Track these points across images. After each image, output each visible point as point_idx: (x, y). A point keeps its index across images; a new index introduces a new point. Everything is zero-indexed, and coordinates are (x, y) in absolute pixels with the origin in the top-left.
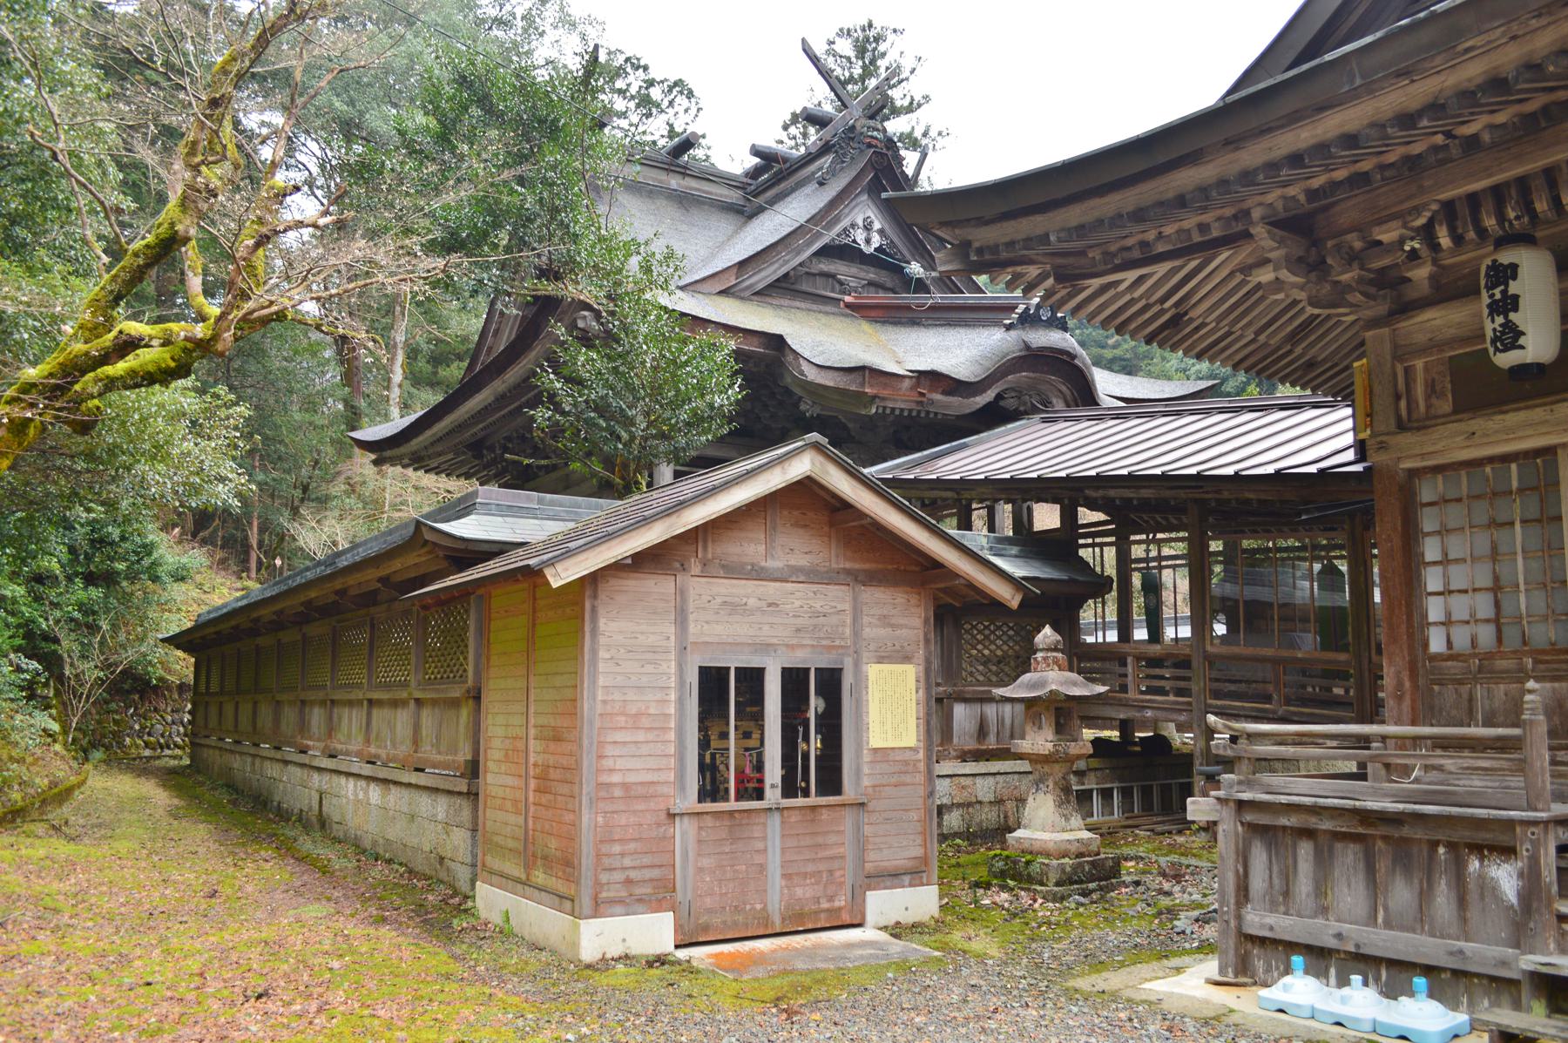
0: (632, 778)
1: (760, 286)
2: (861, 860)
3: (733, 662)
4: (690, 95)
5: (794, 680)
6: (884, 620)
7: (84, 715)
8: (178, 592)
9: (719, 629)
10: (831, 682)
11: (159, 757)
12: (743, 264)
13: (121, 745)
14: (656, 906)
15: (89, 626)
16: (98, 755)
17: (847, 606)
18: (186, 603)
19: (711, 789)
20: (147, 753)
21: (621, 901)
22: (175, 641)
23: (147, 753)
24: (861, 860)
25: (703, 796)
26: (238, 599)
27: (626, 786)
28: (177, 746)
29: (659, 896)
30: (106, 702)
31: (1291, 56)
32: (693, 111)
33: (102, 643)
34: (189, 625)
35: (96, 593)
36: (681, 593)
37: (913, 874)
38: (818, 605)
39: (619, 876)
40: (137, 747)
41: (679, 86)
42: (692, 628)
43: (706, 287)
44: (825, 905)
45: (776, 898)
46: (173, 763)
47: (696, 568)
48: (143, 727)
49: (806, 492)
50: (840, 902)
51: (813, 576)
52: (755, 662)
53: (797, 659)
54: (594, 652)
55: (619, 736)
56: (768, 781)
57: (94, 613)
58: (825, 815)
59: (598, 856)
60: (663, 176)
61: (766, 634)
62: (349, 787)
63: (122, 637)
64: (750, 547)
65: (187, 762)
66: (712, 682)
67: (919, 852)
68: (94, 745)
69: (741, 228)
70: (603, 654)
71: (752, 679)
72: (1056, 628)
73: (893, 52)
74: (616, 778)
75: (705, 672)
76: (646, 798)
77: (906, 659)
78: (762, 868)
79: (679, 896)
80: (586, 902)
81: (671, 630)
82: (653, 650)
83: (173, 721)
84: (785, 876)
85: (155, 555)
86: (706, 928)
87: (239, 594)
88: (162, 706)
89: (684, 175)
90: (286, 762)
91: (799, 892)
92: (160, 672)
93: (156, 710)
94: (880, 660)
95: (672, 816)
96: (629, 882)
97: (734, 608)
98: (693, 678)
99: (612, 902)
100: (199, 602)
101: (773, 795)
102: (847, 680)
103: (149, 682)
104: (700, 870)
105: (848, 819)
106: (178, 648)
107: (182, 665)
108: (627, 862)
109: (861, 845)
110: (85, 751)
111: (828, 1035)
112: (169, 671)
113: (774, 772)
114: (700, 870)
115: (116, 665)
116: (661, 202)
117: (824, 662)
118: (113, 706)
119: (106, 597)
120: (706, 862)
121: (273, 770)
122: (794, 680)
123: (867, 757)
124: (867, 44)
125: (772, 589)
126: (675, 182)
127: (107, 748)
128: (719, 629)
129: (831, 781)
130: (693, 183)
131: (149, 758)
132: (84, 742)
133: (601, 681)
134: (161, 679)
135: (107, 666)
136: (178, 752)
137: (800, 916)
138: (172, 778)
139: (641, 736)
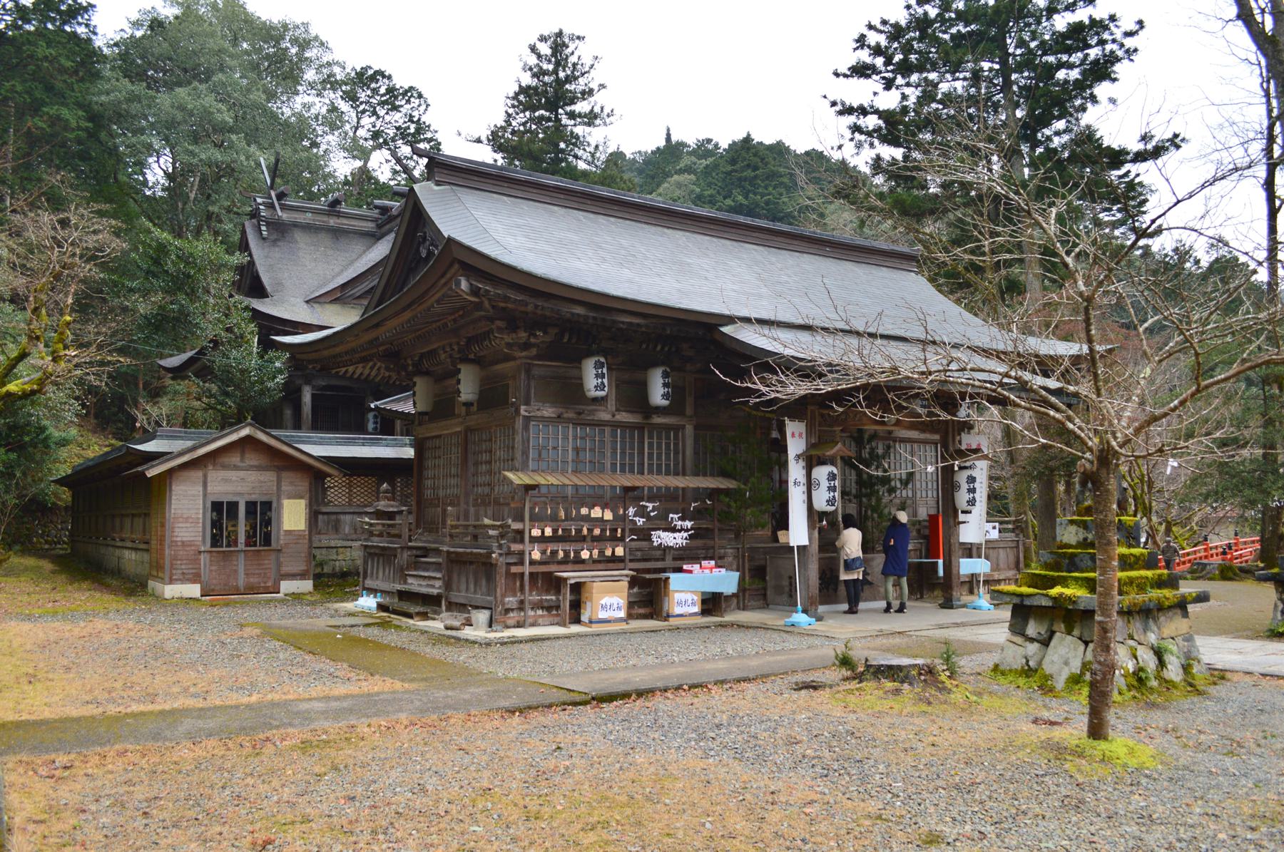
0: (185, 539)
1: (358, 294)
2: (279, 570)
3: (225, 499)
4: (420, 96)
5: (251, 506)
6: (292, 483)
7: (8, 524)
8: (63, 453)
9: (219, 488)
10: (267, 506)
11: (54, 549)
12: (344, 286)
13: (31, 542)
14: (194, 582)
15: (8, 474)
16: (17, 547)
17: (275, 479)
18: (70, 457)
19: (216, 541)
20: (47, 546)
21: (180, 580)
22: (60, 482)
23: (47, 546)
24: (279, 570)
25: (212, 546)
26: (107, 453)
27: (183, 542)
28: (64, 543)
29: (195, 578)
30: (22, 518)
31: (373, 306)
32: (423, 107)
33: (17, 484)
34: (69, 472)
35: (13, 456)
36: (205, 477)
37: (302, 576)
38: (262, 479)
39: (180, 572)
40: (41, 543)
41: (409, 92)
42: (209, 488)
43: (322, 300)
44: (262, 585)
45: (241, 581)
46: (61, 552)
47: (211, 468)
48: (44, 532)
49: (248, 439)
50: (269, 584)
51: (259, 468)
52: (235, 499)
53: (253, 498)
54: (170, 497)
55: (180, 525)
56: (239, 541)
57: (12, 467)
58: (263, 553)
59: (172, 564)
60: (325, 219)
61: (239, 489)
62: (127, 553)
63: (29, 479)
64: (235, 459)
65: (69, 551)
66: (217, 506)
67: (305, 568)
68: (15, 542)
69: (368, 249)
70: (173, 497)
71: (233, 506)
72: (388, 484)
73: (580, 53)
74: (179, 539)
75: (213, 503)
76: (191, 546)
77: (301, 497)
78: (236, 571)
79: (203, 579)
80: (167, 579)
81: (201, 489)
82: (194, 496)
83: (62, 530)
84: (246, 574)
85: (47, 433)
86: (213, 590)
87: (106, 449)
88: (55, 519)
89: (339, 216)
90: (108, 545)
91: (252, 580)
92: (53, 499)
93: (51, 522)
94: (289, 498)
95: (200, 552)
96: (183, 573)
97: (226, 481)
98: (209, 505)
99: (176, 580)
100: (78, 456)
101: (241, 546)
102: (274, 505)
103: (47, 505)
104: (211, 571)
105: (273, 556)
106: (62, 485)
107: (66, 495)
108: (183, 567)
109: (279, 565)
110: (9, 545)
111: (741, 798)
112: (60, 499)
113: (242, 538)
114: (211, 571)
115: (26, 496)
116: (322, 236)
117: (264, 499)
118: (25, 520)
119: (18, 457)
120: (213, 568)
121: (103, 550)
122: (251, 506)
123: (282, 533)
124: (559, 44)
125: (242, 474)
126: (332, 222)
127: (22, 544)
128: (219, 488)
129: (267, 540)
130: (345, 221)
131: (47, 550)
132: (9, 540)
133: (173, 507)
134: (54, 504)
135: (18, 497)
136: (65, 546)
137: (252, 588)
138: (57, 559)
139: (188, 525)
